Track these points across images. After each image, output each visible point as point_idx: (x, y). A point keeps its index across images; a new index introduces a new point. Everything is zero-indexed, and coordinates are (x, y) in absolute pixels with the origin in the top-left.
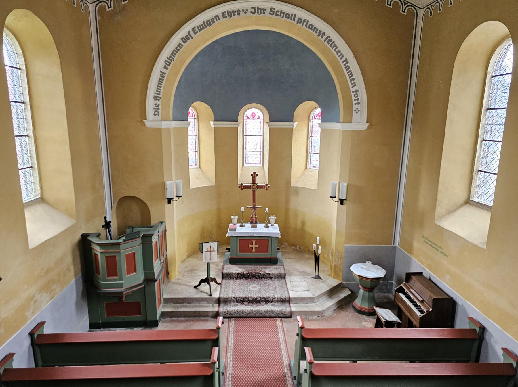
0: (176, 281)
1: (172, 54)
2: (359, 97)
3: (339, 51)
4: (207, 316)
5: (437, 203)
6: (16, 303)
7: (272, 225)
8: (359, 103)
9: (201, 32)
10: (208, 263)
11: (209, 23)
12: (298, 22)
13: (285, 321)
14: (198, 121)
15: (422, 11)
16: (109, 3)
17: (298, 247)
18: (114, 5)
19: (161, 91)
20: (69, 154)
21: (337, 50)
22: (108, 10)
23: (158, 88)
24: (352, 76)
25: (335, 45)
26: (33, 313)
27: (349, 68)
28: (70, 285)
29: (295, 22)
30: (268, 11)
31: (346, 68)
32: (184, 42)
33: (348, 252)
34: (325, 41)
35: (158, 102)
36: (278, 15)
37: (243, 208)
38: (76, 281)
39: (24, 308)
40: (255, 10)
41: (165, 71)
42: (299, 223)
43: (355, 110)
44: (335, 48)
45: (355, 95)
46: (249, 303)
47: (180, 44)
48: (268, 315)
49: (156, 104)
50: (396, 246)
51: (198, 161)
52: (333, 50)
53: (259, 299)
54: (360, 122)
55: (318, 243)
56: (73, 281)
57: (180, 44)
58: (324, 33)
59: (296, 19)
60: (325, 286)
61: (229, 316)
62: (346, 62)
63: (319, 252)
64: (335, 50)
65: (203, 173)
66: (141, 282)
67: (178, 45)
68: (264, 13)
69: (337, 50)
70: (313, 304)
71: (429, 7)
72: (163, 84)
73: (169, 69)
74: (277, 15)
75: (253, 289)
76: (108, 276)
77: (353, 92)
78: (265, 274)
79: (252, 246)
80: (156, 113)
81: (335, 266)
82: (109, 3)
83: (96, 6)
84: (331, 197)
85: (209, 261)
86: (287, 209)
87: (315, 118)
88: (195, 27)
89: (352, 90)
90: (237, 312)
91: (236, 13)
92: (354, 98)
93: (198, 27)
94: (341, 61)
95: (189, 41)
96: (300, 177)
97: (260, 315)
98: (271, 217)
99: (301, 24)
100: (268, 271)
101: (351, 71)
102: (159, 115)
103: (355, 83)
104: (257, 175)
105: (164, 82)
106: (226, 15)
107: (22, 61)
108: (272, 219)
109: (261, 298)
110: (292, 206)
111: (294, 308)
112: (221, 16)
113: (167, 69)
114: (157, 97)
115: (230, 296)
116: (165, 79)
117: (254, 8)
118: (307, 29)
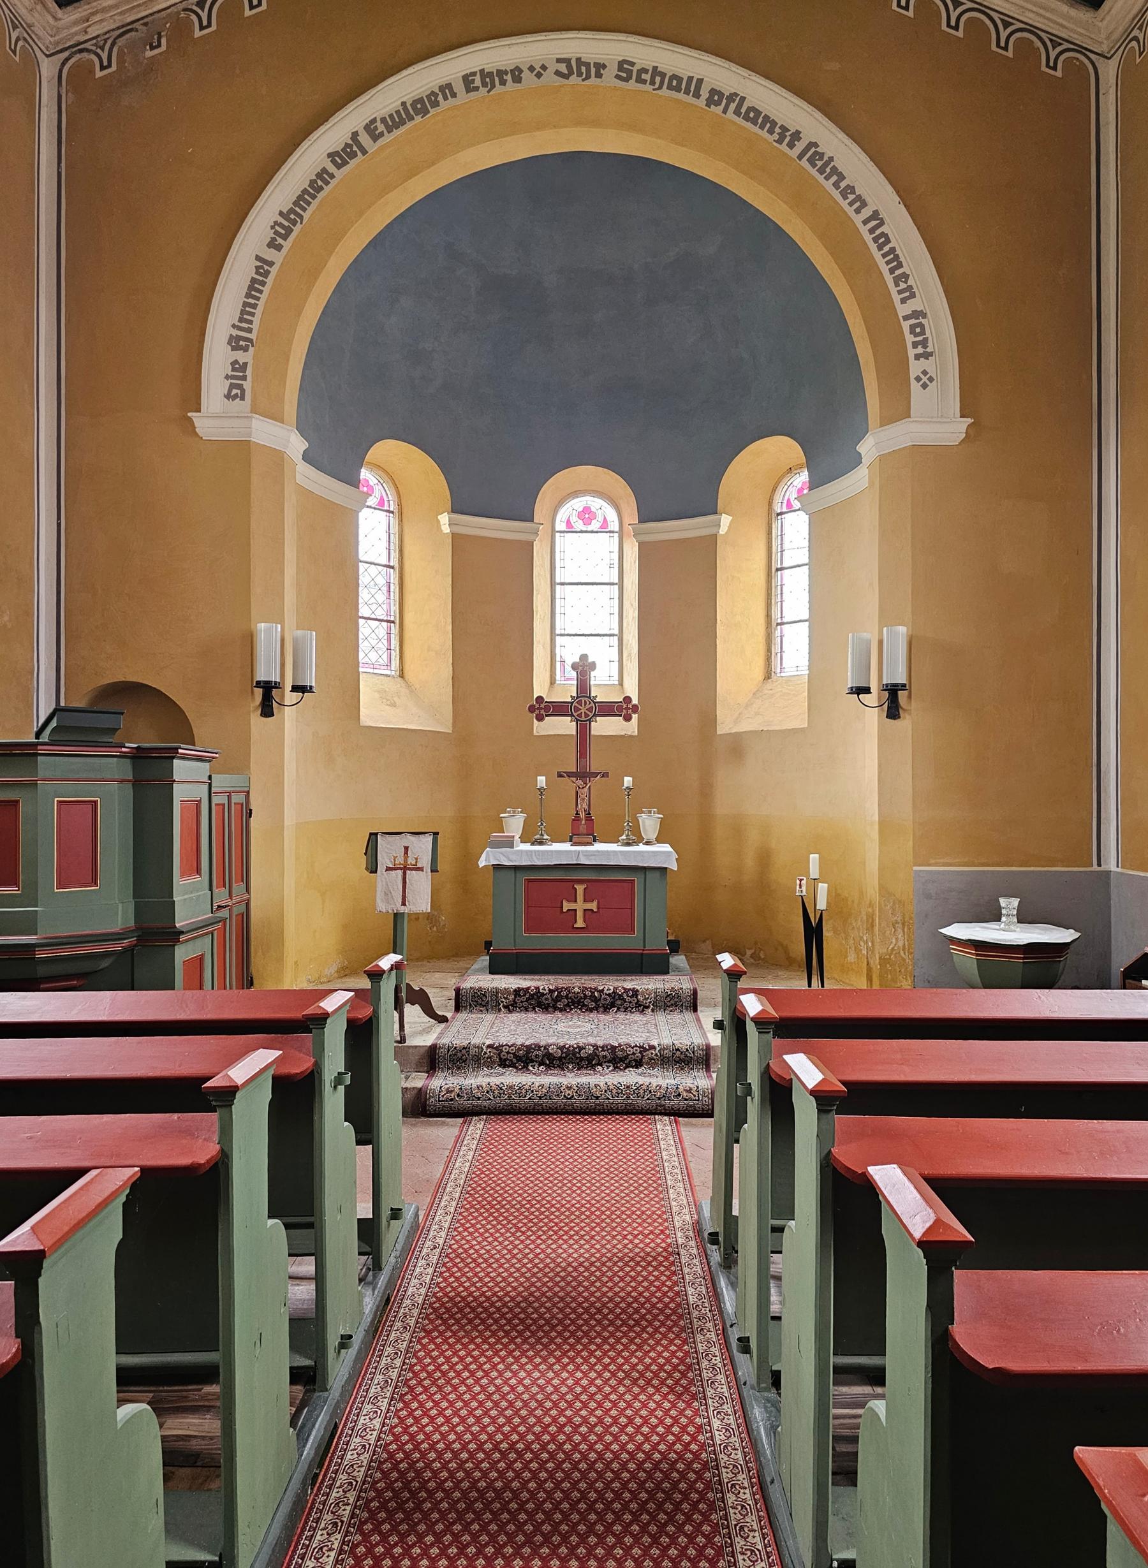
1: (296, 203)
2: (928, 334)
3: (852, 189)
8: (931, 354)
9: (396, 133)
10: (396, 915)
11: (421, 106)
13: (686, 1125)
14: (401, 521)
15: (1113, 63)
16: (105, 56)
17: (749, 953)
18: (121, 61)
19: (256, 320)
21: (843, 185)
22: (99, 74)
23: (247, 311)
24: (900, 265)
25: (834, 169)
27: (888, 241)
29: (702, 102)
30: (611, 71)
31: (875, 240)
32: (339, 167)
34: (800, 157)
35: (241, 357)
36: (644, 82)
40: (569, 67)
41: (270, 254)
42: (750, 861)
43: (918, 379)
44: (835, 178)
45: (912, 328)
46: (548, 1067)
47: (324, 170)
48: (620, 1101)
49: (236, 362)
50: (1108, 873)
51: (395, 655)
52: (828, 185)
54: (936, 417)
55: (814, 872)
57: (324, 170)
59: (705, 93)
63: (822, 904)
64: (836, 185)
65: (412, 692)
66: (116, 927)
68: (599, 75)
69: (843, 185)
71: (1136, 33)
73: (284, 251)
74: (640, 80)
77: (906, 318)
79: (572, 906)
80: (234, 391)
81: (883, 961)
82: (105, 56)
83: (63, 64)
85: (402, 909)
88: (374, 121)
89: (903, 310)
91: (509, 77)
92: (910, 339)
93: (383, 120)
94: (858, 219)
95: (353, 163)
96: (748, 705)
97: (592, 1102)
99: (722, 107)
101: (893, 250)
102: (242, 399)
103: (910, 288)
104: (593, 666)
109: (596, 1047)
110: (723, 806)
112: (459, 87)
113: (279, 248)
114: (239, 338)
115: (476, 1041)
116: (270, 280)
117: (567, 61)
118: (740, 121)
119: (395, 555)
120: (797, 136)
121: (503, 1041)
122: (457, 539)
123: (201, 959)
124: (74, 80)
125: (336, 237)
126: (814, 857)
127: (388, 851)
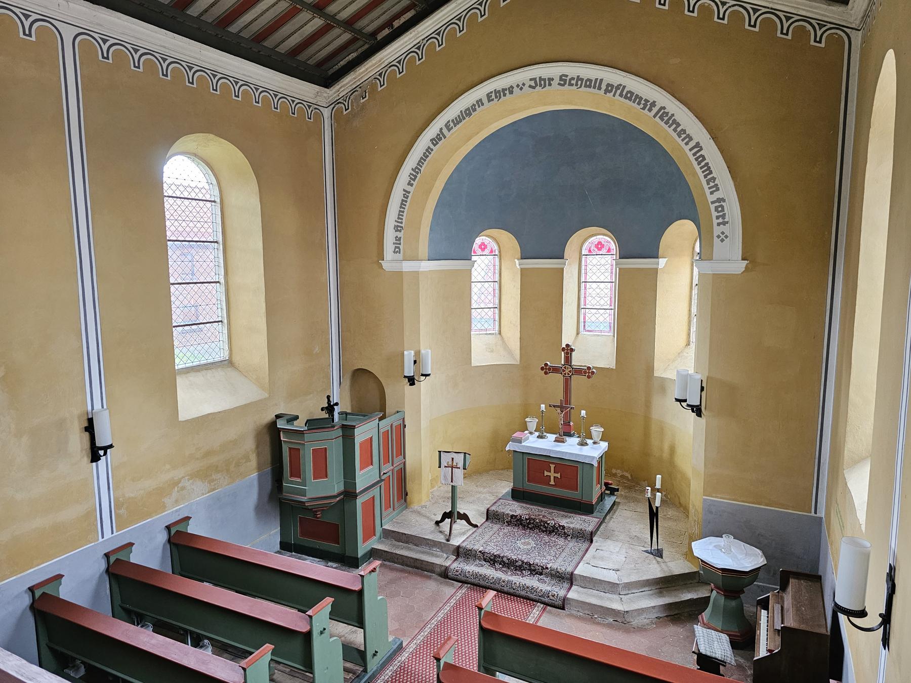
0: (419, 509)
2: (726, 211)
3: (684, 131)
4: (433, 572)
5: (848, 429)
6: (149, 484)
7: (595, 443)
8: (727, 222)
9: (458, 126)
11: (468, 112)
12: (606, 91)
13: (550, 612)
14: (500, 260)
19: (404, 218)
20: (264, 305)
21: (679, 129)
24: (711, 173)
26: (177, 502)
27: (704, 159)
28: (249, 481)
31: (696, 159)
32: (435, 145)
33: (711, 512)
34: (655, 116)
35: (399, 234)
36: (572, 85)
37: (543, 406)
38: (260, 477)
39: (162, 491)
41: (409, 188)
43: (718, 237)
44: (674, 126)
45: (716, 208)
47: (429, 147)
48: (523, 593)
51: (497, 323)
52: (670, 130)
53: (520, 563)
56: (255, 475)
57: (429, 147)
58: (654, 102)
59: (604, 87)
60: (659, 569)
61: (464, 579)
62: (696, 150)
66: (336, 492)
67: (427, 150)
68: (550, 85)
69: (679, 129)
70: (616, 597)
72: (406, 208)
75: (523, 546)
76: (291, 476)
77: (713, 203)
78: (557, 526)
84: (677, 400)
86: (647, 420)
87: (590, 251)
89: (711, 198)
90: (476, 575)
91: (507, 92)
93: (453, 121)
95: (440, 143)
97: (512, 591)
98: (593, 429)
100: (563, 522)
104: (572, 350)
105: (407, 204)
106: (493, 97)
107: (217, 192)
108: (597, 431)
109: (523, 562)
110: (655, 415)
111: (575, 594)
112: (485, 100)
113: (412, 185)
114: (398, 226)
115: (476, 548)
116: (409, 200)
117: (534, 79)
118: (622, 99)
119: (497, 276)
120: (653, 104)
121: (487, 551)
122: (523, 271)
123: (373, 498)
124: (337, 117)
125: (438, 172)
126: (659, 477)
127: (446, 459)
